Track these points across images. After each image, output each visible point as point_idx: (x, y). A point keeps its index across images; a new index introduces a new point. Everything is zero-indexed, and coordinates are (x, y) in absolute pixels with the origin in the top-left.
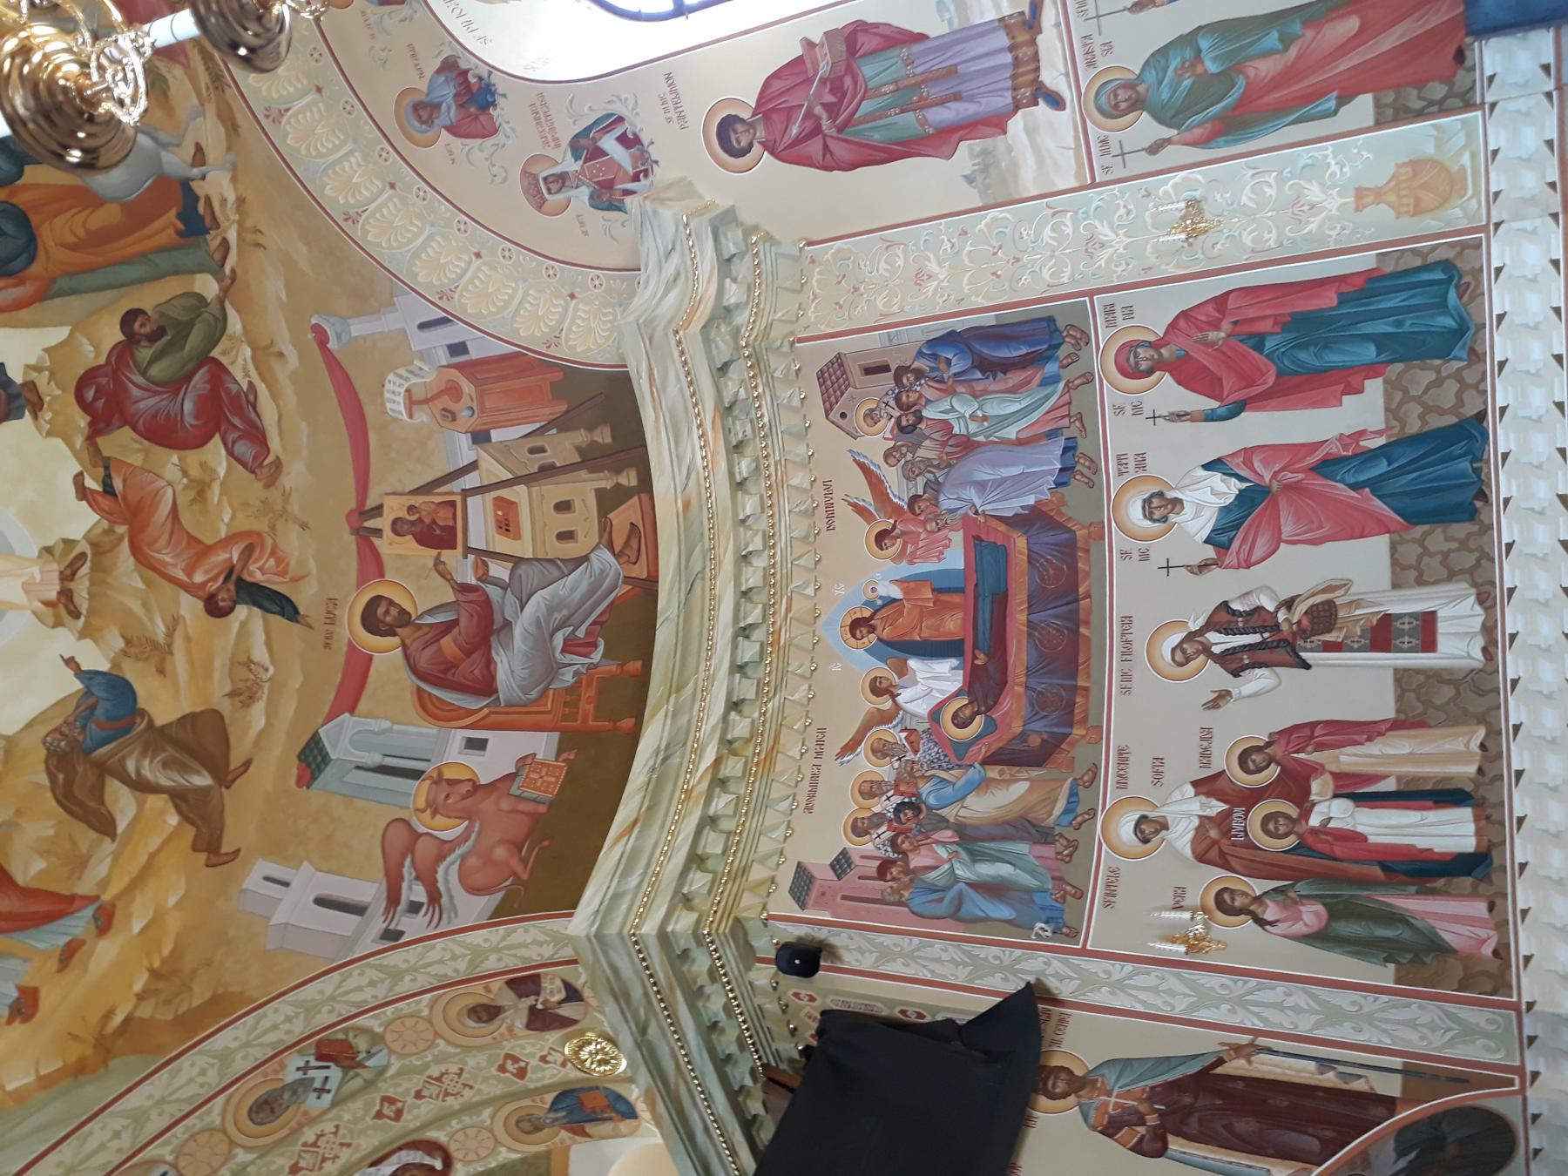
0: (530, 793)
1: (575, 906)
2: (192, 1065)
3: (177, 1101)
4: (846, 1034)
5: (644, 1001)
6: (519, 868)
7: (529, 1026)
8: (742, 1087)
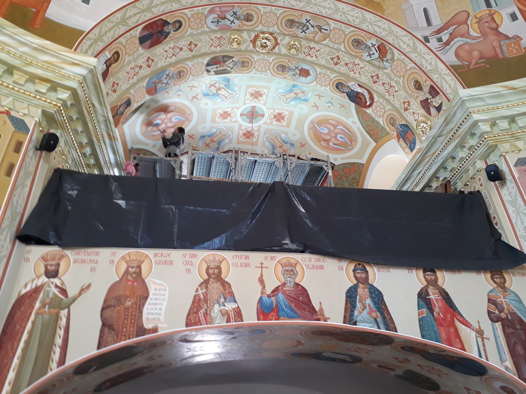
0: (505, 49)
1: (468, 87)
2: (357, 13)
3: (346, 17)
4: (475, 202)
5: (449, 130)
6: (473, 63)
7: (421, 102)
8: (438, 178)
